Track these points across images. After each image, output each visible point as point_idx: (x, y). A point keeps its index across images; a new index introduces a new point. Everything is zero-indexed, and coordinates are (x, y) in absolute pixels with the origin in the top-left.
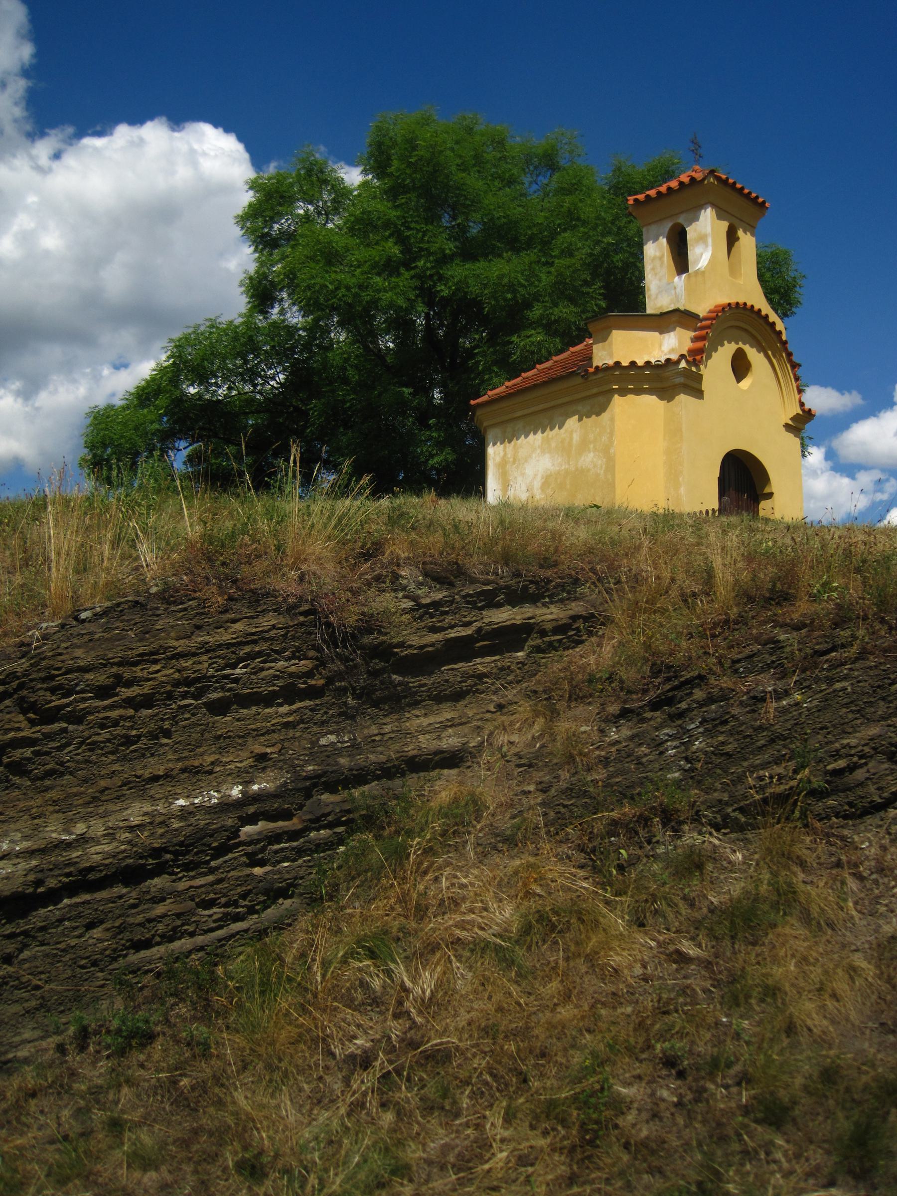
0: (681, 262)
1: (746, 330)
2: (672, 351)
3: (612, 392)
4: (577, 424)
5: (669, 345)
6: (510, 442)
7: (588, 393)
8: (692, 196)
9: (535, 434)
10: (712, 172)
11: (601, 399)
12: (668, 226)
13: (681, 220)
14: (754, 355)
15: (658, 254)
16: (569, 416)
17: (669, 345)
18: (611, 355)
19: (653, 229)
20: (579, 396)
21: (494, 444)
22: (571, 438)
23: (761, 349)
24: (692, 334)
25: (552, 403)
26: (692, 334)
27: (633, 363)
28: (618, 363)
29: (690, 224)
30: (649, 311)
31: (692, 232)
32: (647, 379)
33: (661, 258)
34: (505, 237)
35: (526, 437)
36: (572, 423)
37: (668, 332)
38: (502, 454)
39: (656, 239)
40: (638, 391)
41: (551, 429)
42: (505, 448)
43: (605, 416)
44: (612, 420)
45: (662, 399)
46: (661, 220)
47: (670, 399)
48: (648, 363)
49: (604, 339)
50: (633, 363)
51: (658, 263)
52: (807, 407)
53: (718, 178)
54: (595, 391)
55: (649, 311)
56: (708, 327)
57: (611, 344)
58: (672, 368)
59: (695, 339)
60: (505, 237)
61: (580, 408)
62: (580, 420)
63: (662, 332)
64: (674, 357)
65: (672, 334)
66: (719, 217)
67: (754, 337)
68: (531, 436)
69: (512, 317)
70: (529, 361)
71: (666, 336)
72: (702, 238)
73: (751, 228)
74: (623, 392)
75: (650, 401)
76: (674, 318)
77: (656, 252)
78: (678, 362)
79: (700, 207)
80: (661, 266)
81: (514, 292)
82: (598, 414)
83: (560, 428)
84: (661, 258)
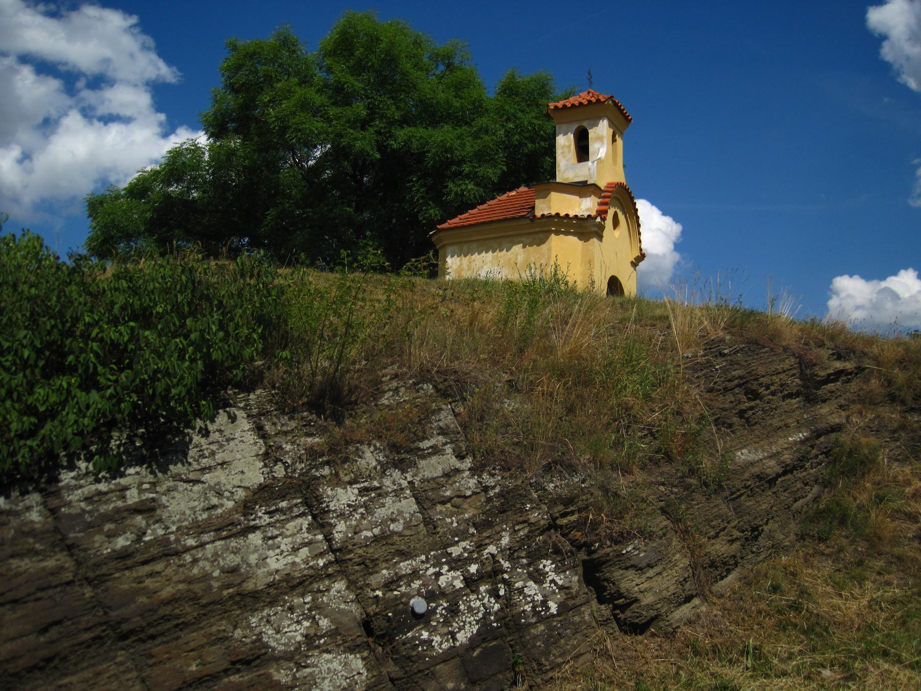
0: (583, 153)
1: (619, 200)
2: (588, 210)
3: (551, 232)
4: (522, 250)
5: (586, 206)
6: (465, 256)
7: (531, 231)
8: (595, 110)
9: (487, 252)
10: (612, 97)
11: (541, 236)
12: (575, 126)
13: (585, 124)
14: (621, 217)
15: (567, 144)
16: (519, 243)
17: (586, 206)
18: (550, 208)
19: (564, 127)
20: (525, 232)
21: (452, 257)
22: (516, 259)
23: (624, 213)
24: (599, 200)
25: (503, 234)
26: (599, 200)
27: (567, 215)
28: (558, 214)
29: (592, 128)
30: (558, 180)
31: (592, 133)
32: (573, 226)
33: (569, 147)
34: (431, 115)
35: (479, 254)
36: (517, 249)
37: (586, 197)
38: (458, 263)
39: (566, 134)
40: (567, 233)
41: (500, 251)
42: (461, 261)
43: (544, 247)
44: (550, 250)
45: (580, 239)
46: (570, 122)
47: (586, 240)
48: (576, 216)
49: (545, 197)
50: (567, 215)
51: (566, 150)
52: (558, 263)
53: (614, 102)
54: (537, 229)
55: (558, 180)
56: (609, 197)
57: (549, 201)
58: (590, 221)
59: (600, 204)
60: (431, 115)
61: (524, 239)
62: (524, 247)
63: (581, 197)
64: (593, 213)
65: (588, 199)
66: (610, 126)
67: (621, 205)
68: (484, 254)
69: (442, 170)
70: (465, 206)
71: (584, 199)
72: (600, 139)
73: (621, 134)
74: (558, 233)
75: (573, 240)
76: (591, 189)
77: (565, 142)
78: (595, 218)
79: (600, 118)
80: (569, 151)
81: (452, 153)
82: (539, 245)
83: (507, 251)
84: (569, 147)
